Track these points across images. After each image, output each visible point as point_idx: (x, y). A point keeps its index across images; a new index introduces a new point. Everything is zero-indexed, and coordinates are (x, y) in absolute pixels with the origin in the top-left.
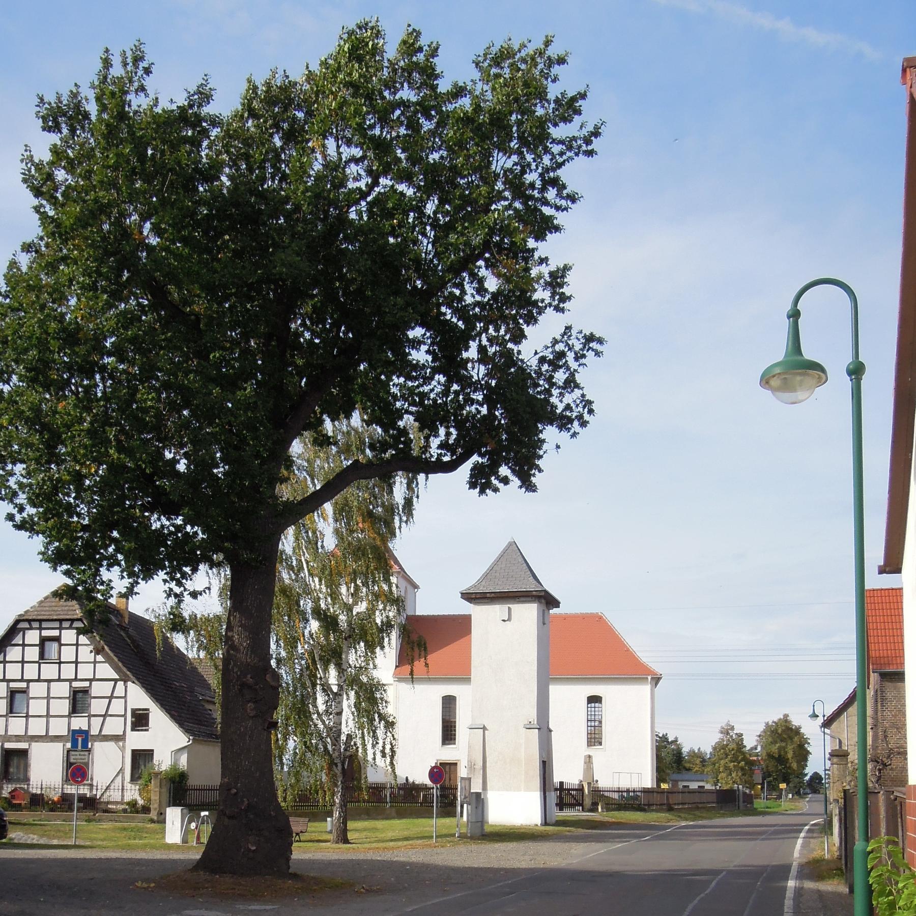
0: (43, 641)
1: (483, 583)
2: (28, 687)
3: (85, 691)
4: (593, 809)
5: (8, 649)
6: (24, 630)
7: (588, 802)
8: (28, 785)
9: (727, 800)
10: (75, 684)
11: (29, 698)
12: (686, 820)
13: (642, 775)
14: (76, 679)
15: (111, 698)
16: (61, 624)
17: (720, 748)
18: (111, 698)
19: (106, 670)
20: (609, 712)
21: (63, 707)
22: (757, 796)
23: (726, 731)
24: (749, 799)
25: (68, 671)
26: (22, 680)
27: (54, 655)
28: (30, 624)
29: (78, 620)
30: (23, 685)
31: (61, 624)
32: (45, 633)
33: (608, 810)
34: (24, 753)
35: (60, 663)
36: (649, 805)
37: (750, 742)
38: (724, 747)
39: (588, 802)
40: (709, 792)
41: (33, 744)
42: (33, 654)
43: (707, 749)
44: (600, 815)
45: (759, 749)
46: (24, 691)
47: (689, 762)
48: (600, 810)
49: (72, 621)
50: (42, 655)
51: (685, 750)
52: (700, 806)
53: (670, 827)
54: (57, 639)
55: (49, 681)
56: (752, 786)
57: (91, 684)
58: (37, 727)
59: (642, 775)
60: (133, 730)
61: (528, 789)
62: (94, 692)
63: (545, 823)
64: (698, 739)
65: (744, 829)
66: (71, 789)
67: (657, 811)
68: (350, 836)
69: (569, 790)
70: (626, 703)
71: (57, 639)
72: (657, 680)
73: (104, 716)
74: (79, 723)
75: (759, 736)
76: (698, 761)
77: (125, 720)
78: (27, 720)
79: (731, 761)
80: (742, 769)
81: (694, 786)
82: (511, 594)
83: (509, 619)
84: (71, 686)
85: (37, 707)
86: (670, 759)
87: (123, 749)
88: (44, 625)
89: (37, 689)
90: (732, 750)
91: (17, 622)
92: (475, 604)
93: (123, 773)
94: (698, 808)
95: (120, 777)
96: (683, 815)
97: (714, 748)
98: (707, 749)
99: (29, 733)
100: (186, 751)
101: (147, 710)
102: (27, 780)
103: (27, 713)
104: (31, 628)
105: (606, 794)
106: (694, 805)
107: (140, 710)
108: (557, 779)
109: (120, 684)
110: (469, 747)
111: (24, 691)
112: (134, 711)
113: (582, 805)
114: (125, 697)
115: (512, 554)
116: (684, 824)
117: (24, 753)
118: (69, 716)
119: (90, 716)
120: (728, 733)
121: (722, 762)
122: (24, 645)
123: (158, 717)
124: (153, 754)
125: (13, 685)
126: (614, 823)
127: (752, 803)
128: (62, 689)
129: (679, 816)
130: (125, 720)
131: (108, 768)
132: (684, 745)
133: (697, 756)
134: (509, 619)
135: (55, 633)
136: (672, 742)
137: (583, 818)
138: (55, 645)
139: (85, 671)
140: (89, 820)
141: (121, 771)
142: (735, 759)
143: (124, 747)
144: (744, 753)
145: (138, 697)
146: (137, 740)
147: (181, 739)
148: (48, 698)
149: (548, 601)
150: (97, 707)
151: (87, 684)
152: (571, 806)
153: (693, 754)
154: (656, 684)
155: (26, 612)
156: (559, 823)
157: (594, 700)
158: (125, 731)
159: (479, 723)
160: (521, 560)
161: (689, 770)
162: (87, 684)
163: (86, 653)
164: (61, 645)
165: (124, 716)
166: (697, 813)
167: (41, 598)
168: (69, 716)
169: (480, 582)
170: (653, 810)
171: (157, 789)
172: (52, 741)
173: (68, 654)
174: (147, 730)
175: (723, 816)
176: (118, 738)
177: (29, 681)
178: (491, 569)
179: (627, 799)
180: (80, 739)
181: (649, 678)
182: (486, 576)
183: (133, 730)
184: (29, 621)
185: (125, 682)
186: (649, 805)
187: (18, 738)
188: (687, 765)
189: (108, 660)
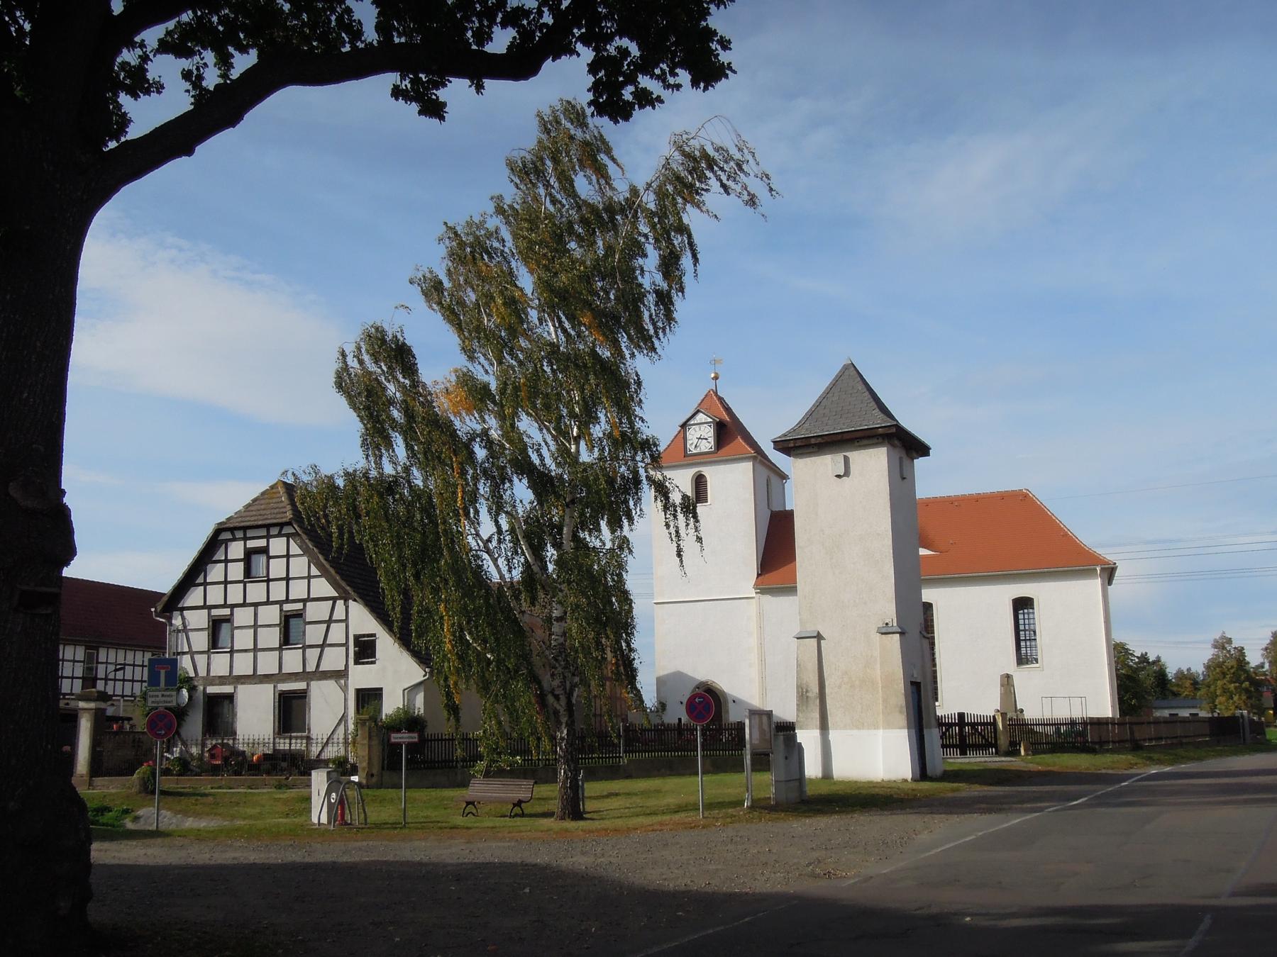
0: (249, 554)
1: (806, 425)
2: (232, 614)
3: (299, 615)
4: (1013, 752)
5: (209, 566)
6: (226, 542)
7: (1003, 741)
8: (234, 739)
9: (1227, 734)
10: (287, 607)
11: (233, 629)
12: (1160, 762)
13: (1100, 702)
14: (287, 601)
15: (329, 622)
16: (268, 531)
17: (1212, 666)
18: (329, 622)
19: (322, 587)
20: (1043, 619)
21: (271, 637)
22: (1269, 724)
23: (1222, 644)
24: (1258, 728)
25: (278, 591)
26: (225, 606)
27: (262, 572)
28: (233, 534)
29: (289, 524)
30: (227, 611)
31: (268, 531)
32: (252, 544)
33: (1035, 752)
34: (230, 698)
35: (268, 581)
36: (1102, 743)
37: (1255, 658)
38: (1220, 665)
39: (1003, 741)
40: (1204, 720)
41: (240, 687)
42: (236, 571)
43: (1198, 668)
44: (1024, 761)
45: (1267, 666)
46: (228, 620)
47: (1178, 685)
48: (1023, 753)
49: (281, 525)
50: (248, 572)
51: (1171, 671)
52: (1184, 740)
53: (1132, 776)
54: (264, 551)
55: (256, 605)
56: (1261, 711)
57: (305, 606)
58: (243, 665)
59: (1100, 702)
60: (357, 662)
61: (889, 725)
62: (310, 616)
63: (922, 773)
64: (1185, 655)
65: (1254, 780)
66: (283, 745)
67: (1112, 751)
68: (589, 806)
69: (973, 725)
70: (1067, 607)
71: (264, 551)
72: (1109, 573)
73: (322, 646)
74: (292, 660)
75: (1266, 649)
76: (1188, 684)
77: (347, 650)
78: (232, 657)
79: (1231, 682)
80: (1247, 690)
81: (1185, 713)
82: (846, 437)
83: (847, 473)
84: (281, 610)
85: (243, 639)
86: (1137, 681)
87: (345, 689)
88: (250, 533)
89: (243, 617)
90: (1230, 666)
91: (219, 531)
92: (797, 456)
93: (346, 722)
94: (1181, 744)
95: (342, 726)
96: (1156, 756)
97: (1208, 667)
98: (1198, 668)
99: (235, 673)
100: (422, 688)
101: (374, 635)
102: (233, 733)
103: (232, 647)
104: (234, 539)
105: (1039, 729)
106: (1175, 741)
107: (364, 636)
108: (947, 706)
109: (340, 603)
110: (798, 665)
111: (228, 620)
112: (357, 637)
113: (995, 746)
114: (346, 620)
115: (851, 381)
116: (1154, 771)
117: (230, 698)
118: (280, 649)
119: (304, 648)
120: (1224, 648)
121: (1219, 683)
122: (226, 561)
123: (386, 645)
124: (381, 695)
125: (215, 612)
126: (1039, 773)
127: (1264, 734)
128: (271, 615)
129: (1150, 759)
130: (347, 650)
131: (328, 712)
132: (1168, 665)
133: (1186, 677)
134: (847, 473)
135: (262, 543)
136: (1154, 662)
137: (993, 766)
138: (263, 558)
139: (298, 590)
140: (279, 787)
141: (344, 718)
142: (1236, 679)
143: (346, 685)
144: (1247, 672)
145: (362, 620)
146: (362, 676)
147: (414, 672)
148: (255, 626)
149: (909, 446)
150: (314, 634)
151: (299, 606)
152: (977, 747)
153: (1181, 675)
154: (1110, 583)
155: (228, 519)
156: (949, 776)
157: (1022, 605)
158: (347, 665)
159: (811, 629)
160: (861, 387)
161: (1176, 695)
162: (299, 606)
163: (300, 565)
164: (269, 558)
165: (346, 645)
166: (1180, 751)
167: (248, 501)
168: (280, 649)
169: (801, 424)
170: (1108, 751)
171: (366, 742)
172: (261, 682)
173: (277, 568)
174: (373, 663)
175: (1221, 754)
176: (340, 675)
177: (233, 606)
178: (819, 404)
179: (1067, 734)
180: (163, 673)
181: (1098, 569)
182: (810, 415)
183: (357, 662)
184: (232, 530)
185: (346, 601)
186: (1102, 743)
187: (222, 680)
188: (1175, 689)
189: (324, 574)
